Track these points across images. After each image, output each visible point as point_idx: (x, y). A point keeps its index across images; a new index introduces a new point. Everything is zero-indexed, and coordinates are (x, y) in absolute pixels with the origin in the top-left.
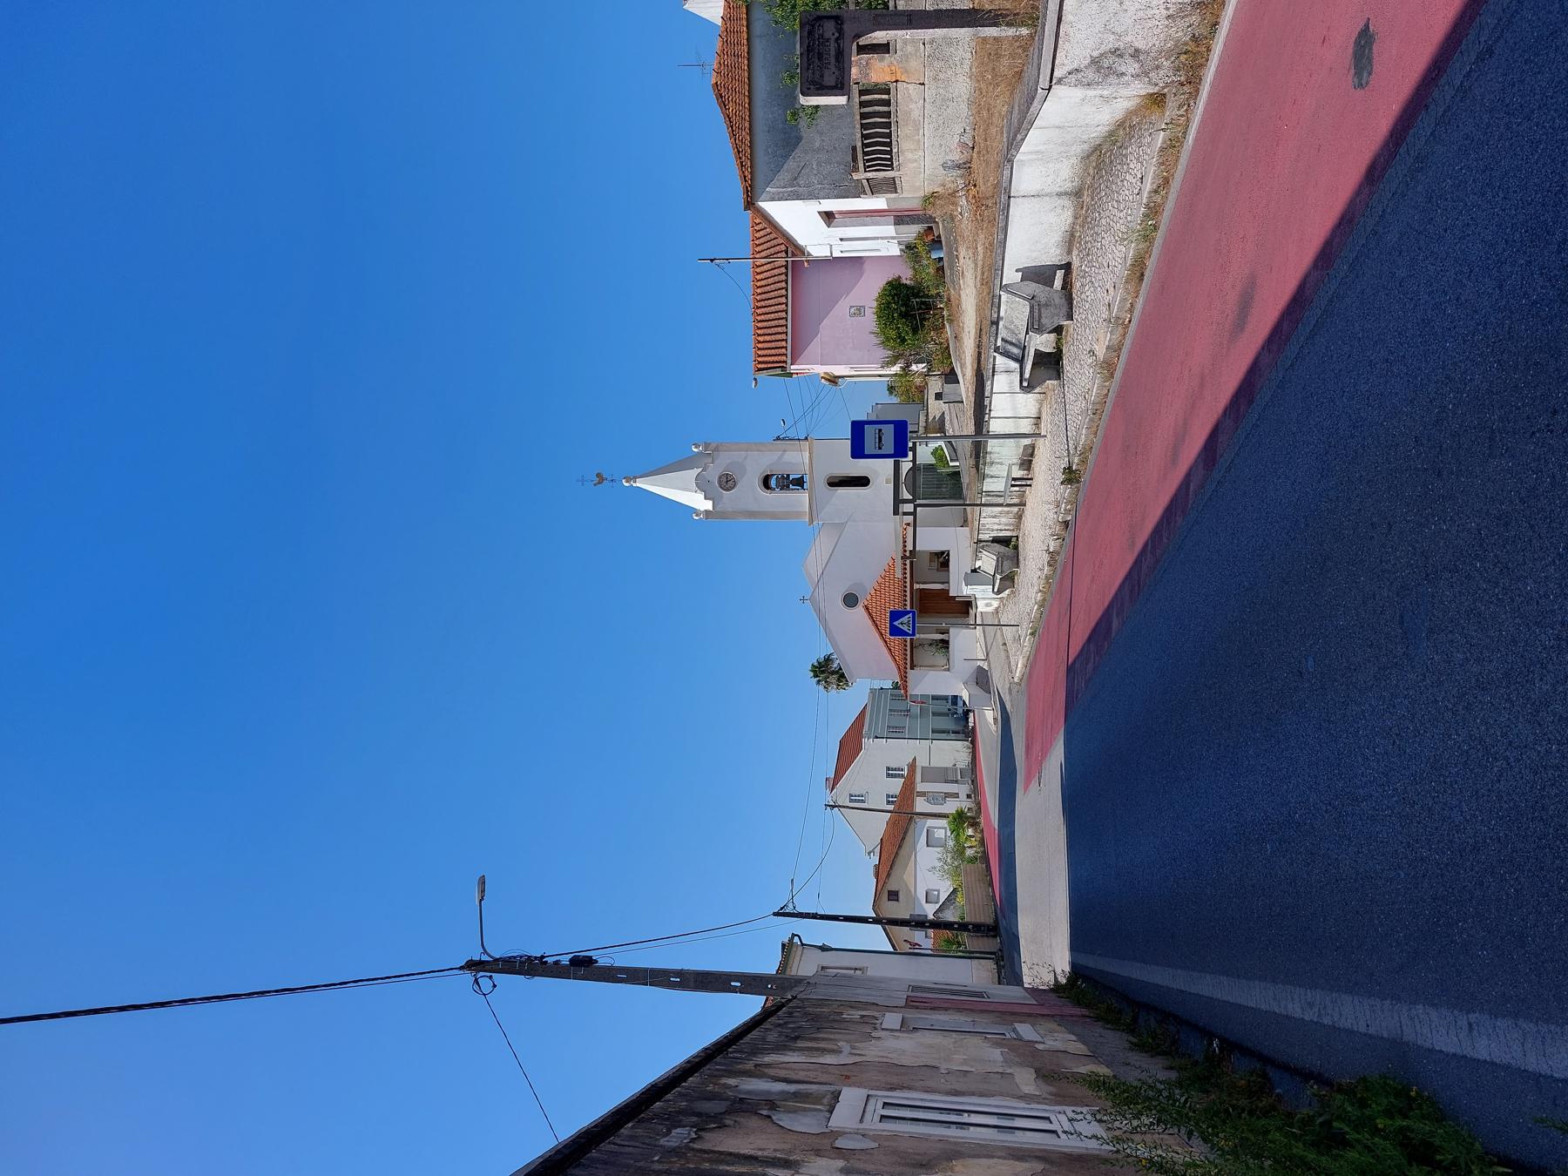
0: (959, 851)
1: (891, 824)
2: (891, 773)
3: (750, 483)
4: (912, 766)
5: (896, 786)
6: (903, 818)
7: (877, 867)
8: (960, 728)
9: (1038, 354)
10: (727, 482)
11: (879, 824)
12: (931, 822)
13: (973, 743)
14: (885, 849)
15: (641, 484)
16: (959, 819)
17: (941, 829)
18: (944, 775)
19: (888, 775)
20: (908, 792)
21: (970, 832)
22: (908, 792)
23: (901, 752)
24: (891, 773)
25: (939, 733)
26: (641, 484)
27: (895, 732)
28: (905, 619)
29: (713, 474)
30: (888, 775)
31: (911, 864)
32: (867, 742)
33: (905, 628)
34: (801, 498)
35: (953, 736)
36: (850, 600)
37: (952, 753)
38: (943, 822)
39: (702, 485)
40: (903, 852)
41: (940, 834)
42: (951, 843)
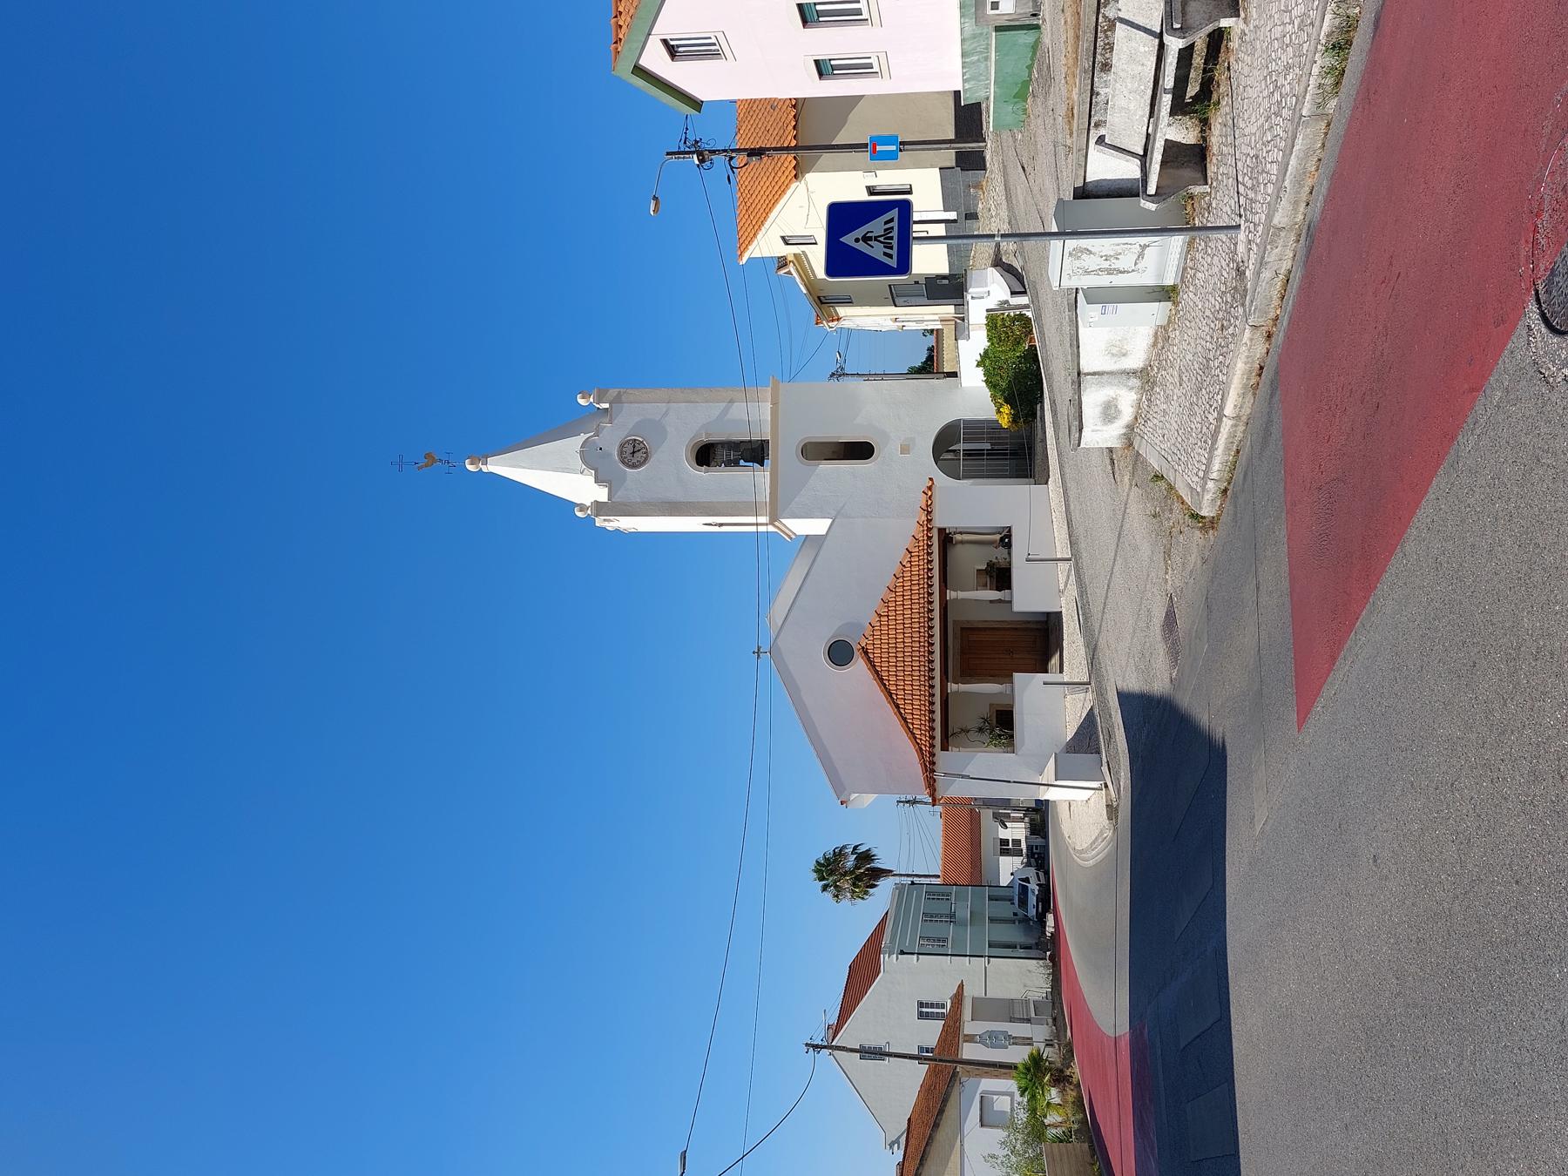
0: (1036, 1131)
1: (928, 1089)
2: (925, 1011)
3: (673, 456)
4: (958, 998)
5: (931, 1033)
6: (945, 1070)
7: (902, 1165)
8: (1032, 941)
9: (1170, 146)
10: (634, 453)
11: (906, 1083)
12: (988, 1084)
13: (1055, 961)
14: (914, 1133)
15: (498, 466)
16: (1035, 1073)
17: (1005, 1093)
18: (1009, 1010)
19: (921, 1016)
20: (952, 1033)
21: (1054, 1095)
22: (952, 1033)
23: (938, 976)
24: (925, 1011)
25: (1002, 948)
26: (498, 466)
27: (936, 946)
28: (876, 226)
29: (612, 437)
30: (921, 1016)
31: (955, 1157)
32: (888, 961)
33: (876, 251)
34: (755, 479)
35: (1021, 952)
36: (839, 653)
37: (1022, 978)
38: (1011, 1085)
39: (591, 459)
40: (941, 1135)
41: (1002, 1104)
42: (1023, 1116)
